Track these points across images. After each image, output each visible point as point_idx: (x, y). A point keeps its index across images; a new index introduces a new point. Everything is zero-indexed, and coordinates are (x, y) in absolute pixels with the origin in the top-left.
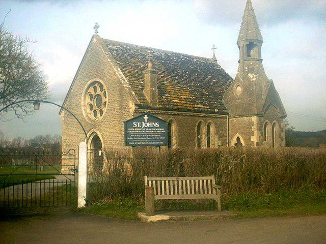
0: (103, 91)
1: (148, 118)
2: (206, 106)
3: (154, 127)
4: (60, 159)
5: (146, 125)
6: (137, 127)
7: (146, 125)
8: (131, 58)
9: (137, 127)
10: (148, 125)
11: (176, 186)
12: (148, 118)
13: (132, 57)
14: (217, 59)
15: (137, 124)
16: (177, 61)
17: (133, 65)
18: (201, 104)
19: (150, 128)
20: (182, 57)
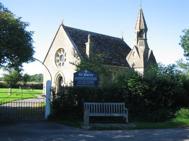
0: (65, 53)
1: (87, 71)
2: (118, 62)
3: (91, 77)
4: (29, 107)
5: (86, 75)
6: (81, 76)
7: (86, 75)
8: (80, 36)
9: (81, 76)
10: (87, 75)
11: (102, 110)
12: (87, 71)
13: (80, 36)
14: (136, 35)
15: (81, 75)
16: (103, 39)
17: (123, 65)
18: (115, 61)
19: (88, 77)
20: (106, 37)
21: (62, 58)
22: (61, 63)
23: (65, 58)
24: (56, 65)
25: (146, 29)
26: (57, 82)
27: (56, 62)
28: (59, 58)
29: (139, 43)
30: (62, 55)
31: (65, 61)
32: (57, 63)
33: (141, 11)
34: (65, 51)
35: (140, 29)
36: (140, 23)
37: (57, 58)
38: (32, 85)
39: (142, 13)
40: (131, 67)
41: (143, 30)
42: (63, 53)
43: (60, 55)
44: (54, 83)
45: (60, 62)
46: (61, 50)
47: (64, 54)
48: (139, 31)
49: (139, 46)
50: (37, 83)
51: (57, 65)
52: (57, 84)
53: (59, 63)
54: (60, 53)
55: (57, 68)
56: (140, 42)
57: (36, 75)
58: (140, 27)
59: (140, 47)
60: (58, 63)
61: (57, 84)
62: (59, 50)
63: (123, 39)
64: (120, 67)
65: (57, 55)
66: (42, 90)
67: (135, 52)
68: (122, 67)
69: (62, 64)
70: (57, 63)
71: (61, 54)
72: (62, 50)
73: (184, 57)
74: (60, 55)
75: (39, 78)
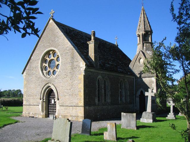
0: (56, 57)
21: (51, 65)
22: (49, 71)
23: (57, 63)
24: (44, 76)
25: (151, 32)
26: (44, 98)
27: (42, 70)
28: (47, 65)
29: (145, 48)
30: (52, 60)
31: (57, 68)
32: (44, 72)
33: (143, 11)
34: (58, 53)
35: (145, 31)
36: (144, 24)
37: (44, 64)
38: (4, 101)
39: (145, 13)
40: (138, 76)
41: (149, 31)
42: (54, 57)
43: (48, 59)
44: (41, 99)
45: (49, 69)
46: (51, 52)
47: (55, 59)
48: (144, 33)
49: (146, 50)
50: (9, 99)
51: (45, 74)
52: (44, 100)
53: (47, 71)
54: (49, 57)
55: (43, 76)
56: (146, 46)
57: (6, 91)
58: (145, 29)
59: (147, 52)
60: (45, 72)
61: (44, 100)
62: (48, 53)
63: (118, 45)
64: (127, 76)
65: (44, 60)
66: (21, 107)
67: (141, 58)
68: (128, 76)
69: (52, 71)
70: (44, 72)
71: (51, 59)
72: (53, 52)
73: (139, 72)
74: (48, 59)
75: (8, 94)
